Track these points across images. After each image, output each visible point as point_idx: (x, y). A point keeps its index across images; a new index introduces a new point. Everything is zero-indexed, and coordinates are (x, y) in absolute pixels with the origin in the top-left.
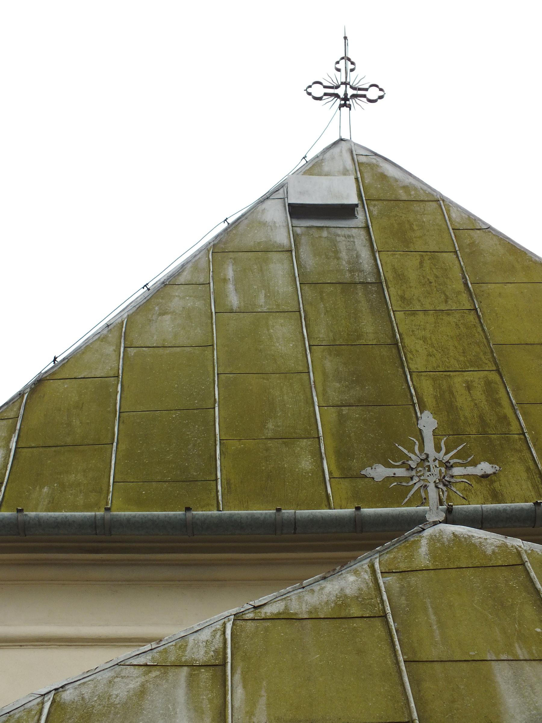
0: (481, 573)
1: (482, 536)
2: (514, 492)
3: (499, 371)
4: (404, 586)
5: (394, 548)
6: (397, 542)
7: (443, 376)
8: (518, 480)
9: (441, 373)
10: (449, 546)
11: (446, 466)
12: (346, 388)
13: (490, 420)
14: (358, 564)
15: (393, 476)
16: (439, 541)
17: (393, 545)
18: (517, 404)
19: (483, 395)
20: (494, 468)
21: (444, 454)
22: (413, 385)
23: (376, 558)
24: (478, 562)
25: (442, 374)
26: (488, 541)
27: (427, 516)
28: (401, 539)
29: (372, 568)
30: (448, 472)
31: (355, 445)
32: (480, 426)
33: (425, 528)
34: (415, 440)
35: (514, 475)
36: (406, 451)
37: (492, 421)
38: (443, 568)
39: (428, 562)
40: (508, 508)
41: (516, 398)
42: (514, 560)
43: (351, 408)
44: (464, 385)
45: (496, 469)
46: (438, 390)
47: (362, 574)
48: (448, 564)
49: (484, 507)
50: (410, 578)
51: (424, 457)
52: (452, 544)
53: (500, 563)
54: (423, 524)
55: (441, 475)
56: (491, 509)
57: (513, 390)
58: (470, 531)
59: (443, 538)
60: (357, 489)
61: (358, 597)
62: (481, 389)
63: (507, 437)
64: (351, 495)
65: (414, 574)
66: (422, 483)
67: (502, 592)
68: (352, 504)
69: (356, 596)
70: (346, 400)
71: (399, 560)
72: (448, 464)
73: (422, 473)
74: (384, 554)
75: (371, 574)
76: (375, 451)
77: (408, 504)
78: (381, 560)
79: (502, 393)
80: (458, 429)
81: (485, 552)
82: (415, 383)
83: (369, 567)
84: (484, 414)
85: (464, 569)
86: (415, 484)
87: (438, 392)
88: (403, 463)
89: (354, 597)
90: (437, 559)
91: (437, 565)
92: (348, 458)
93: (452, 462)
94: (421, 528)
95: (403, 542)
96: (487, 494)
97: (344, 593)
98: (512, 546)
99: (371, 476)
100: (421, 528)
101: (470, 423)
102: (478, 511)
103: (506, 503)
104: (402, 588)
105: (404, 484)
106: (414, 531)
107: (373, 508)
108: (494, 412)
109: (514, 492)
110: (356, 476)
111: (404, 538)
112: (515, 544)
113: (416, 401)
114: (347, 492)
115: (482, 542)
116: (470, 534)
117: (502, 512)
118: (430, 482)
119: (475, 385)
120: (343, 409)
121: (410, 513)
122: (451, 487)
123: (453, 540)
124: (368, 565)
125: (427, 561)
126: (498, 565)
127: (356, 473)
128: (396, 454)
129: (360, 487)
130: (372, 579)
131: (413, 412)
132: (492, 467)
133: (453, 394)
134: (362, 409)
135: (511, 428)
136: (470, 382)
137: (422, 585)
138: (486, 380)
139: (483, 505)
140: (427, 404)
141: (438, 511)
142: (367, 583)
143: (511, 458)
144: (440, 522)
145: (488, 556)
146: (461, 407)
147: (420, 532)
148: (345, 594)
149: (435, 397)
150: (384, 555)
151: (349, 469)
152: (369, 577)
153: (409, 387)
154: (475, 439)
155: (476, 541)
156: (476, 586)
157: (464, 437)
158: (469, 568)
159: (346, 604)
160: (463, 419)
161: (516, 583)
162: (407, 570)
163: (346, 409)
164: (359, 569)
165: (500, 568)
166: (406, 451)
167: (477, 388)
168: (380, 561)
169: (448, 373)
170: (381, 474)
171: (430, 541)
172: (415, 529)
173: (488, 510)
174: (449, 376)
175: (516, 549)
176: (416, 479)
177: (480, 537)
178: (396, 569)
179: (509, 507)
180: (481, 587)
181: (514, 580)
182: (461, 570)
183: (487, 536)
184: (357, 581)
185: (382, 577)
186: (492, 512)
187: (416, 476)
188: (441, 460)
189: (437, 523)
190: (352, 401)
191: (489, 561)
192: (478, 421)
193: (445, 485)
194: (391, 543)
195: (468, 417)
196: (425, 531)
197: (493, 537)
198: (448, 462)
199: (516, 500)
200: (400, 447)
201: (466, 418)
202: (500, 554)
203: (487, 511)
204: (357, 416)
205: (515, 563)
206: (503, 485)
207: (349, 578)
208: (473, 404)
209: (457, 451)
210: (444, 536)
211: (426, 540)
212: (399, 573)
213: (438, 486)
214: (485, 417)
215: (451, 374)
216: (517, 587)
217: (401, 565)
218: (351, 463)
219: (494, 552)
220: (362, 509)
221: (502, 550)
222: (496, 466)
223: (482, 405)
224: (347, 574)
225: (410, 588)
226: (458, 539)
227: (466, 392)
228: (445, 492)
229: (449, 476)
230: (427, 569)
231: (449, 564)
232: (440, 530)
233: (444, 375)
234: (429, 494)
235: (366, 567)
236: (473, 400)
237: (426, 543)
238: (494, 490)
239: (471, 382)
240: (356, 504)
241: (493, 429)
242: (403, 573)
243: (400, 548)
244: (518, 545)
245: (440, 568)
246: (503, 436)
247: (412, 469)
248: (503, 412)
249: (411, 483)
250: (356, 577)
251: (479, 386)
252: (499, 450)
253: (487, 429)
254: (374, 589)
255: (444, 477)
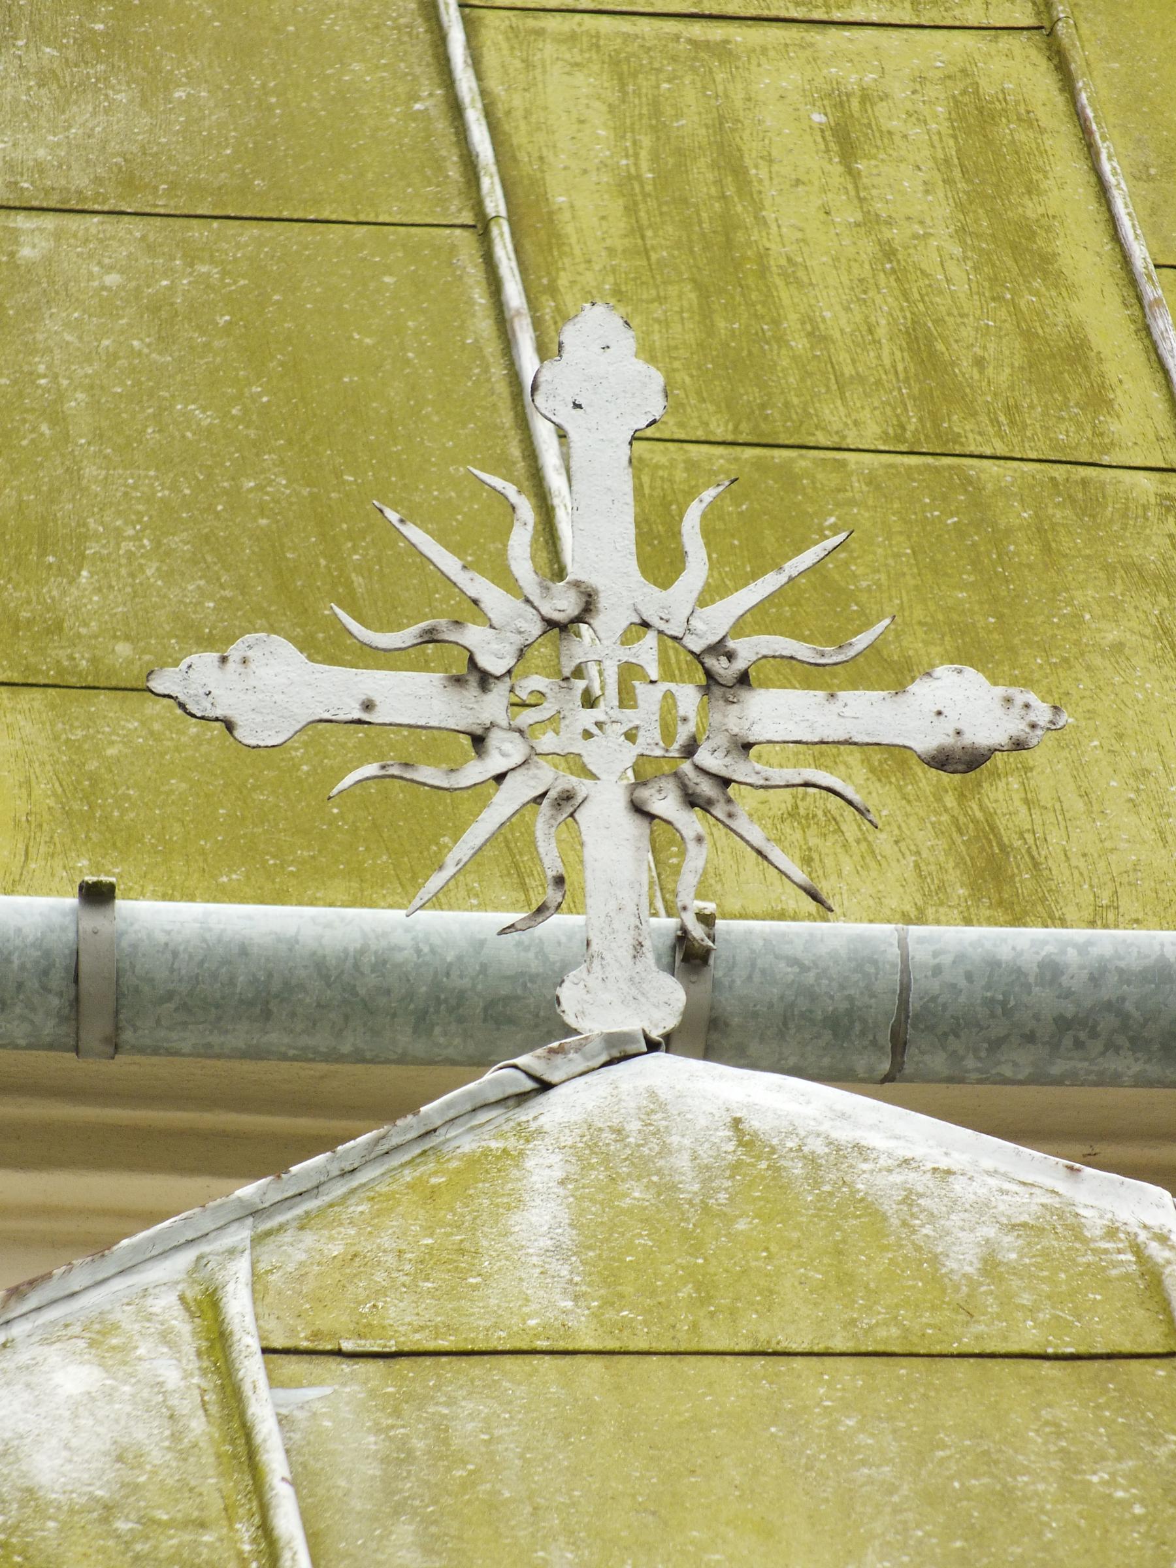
0: (908, 1401)
1: (917, 1152)
2: (1114, 850)
3: (1052, 33)
4: (410, 1452)
5: (353, 1191)
6: (379, 1154)
7: (683, 46)
8: (1146, 772)
9: (671, 26)
10: (706, 1209)
11: (709, 674)
12: (40, 85)
13: (980, 363)
14: (118, 1285)
15: (359, 722)
16: (641, 1166)
17: (343, 1174)
18: (1157, 266)
19: (941, 195)
20: (1017, 710)
21: (695, 594)
22: (483, 93)
23: (232, 1252)
24: (886, 1324)
25: (677, 38)
26: (958, 1185)
27: (564, 993)
28: (395, 1141)
29: (210, 1315)
30: (716, 718)
31: (90, 471)
32: (910, 396)
33: (552, 1078)
34: (511, 491)
35: (1120, 737)
36: (449, 563)
37: (990, 371)
38: (662, 1347)
39: (569, 1304)
40: (1072, 953)
41: (1153, 230)
42: (1123, 1321)
43: (73, 223)
44: (818, 118)
45: (1032, 717)
46: (646, 141)
47: (141, 1351)
48: (694, 1327)
49: (920, 940)
50: (451, 1402)
51: (564, 604)
52: (723, 1197)
53: (1029, 1338)
54: (540, 1051)
55: (668, 734)
56: (960, 958)
57: (1140, 175)
58: (843, 1116)
59: (665, 1150)
60: (92, 765)
61: (108, 1510)
62: (926, 153)
63: (1084, 482)
64: (51, 802)
65: (477, 1372)
66: (544, 777)
67: (1040, 1534)
68: (58, 863)
69: (97, 1500)
70: (40, 167)
71: (380, 1277)
72: (718, 665)
73: (546, 711)
74: (281, 1228)
75: (199, 1354)
76: (217, 515)
77: (436, 902)
78: (263, 1266)
79: (1061, 187)
80: (763, 406)
81: (935, 1260)
82: (496, 86)
83: (187, 1308)
84: (939, 321)
85: (798, 1363)
86: (500, 778)
87: (643, 154)
88: (430, 637)
89: (85, 1510)
90: (628, 1290)
91: (624, 1325)
92: (43, 553)
93: (747, 650)
94: (530, 1076)
95: (407, 1157)
96: (942, 859)
97: (24, 1475)
98: (1112, 1232)
99: (219, 712)
100: (530, 1076)
101: (848, 371)
102: (874, 962)
103: (1063, 923)
104: (399, 1462)
105: (428, 774)
106: (480, 1091)
107: (191, 898)
108: (1003, 313)
109: (1114, 850)
110: (90, 680)
111: (413, 1134)
112: (1132, 1221)
113: (495, 203)
114: (28, 781)
115: (921, 1190)
116: (844, 1134)
117: (1031, 980)
118: (594, 777)
119: (886, 125)
120: (16, 229)
121: (433, 951)
122: (730, 815)
123: (736, 1167)
124: (182, 1298)
125: (565, 1292)
126: (1015, 1348)
127: (94, 660)
128: (354, 549)
129: (111, 751)
130: (203, 1392)
131: (474, 273)
132: (1008, 700)
133: (739, 172)
134: (144, 238)
135: (1114, 426)
136: (855, 103)
137: (527, 1449)
138: (964, 92)
139: (915, 930)
140: (570, 229)
141: (640, 967)
142: (171, 1417)
143: (1103, 625)
144: (652, 1046)
145: (957, 1289)
146: (789, 260)
147: (522, 1098)
148: (27, 1483)
149: (626, 184)
150: (287, 1237)
151: (48, 631)
152: (187, 1375)
153: (456, 109)
154: (872, 480)
155: (883, 1180)
156: (870, 1481)
157: (804, 461)
158: (828, 1361)
159: (31, 1551)
160: (800, 344)
161: (1133, 1479)
162: (431, 1346)
163: (41, 230)
164: (124, 1317)
165: (1025, 1366)
166: (449, 563)
167: (897, 138)
168: (257, 1279)
169: (717, 32)
170: (278, 697)
171: (587, 1167)
172: (490, 1082)
173: (946, 960)
174: (722, 51)
175: (1138, 1250)
176: (507, 747)
177: (906, 1162)
178: (360, 1336)
179: (1082, 949)
180: (905, 1489)
181: (1119, 1459)
182: (782, 1364)
183: (955, 1155)
184: (109, 1395)
185: (270, 1377)
186: (969, 977)
187: (511, 729)
188: (675, 629)
189: (632, 1049)
190: (81, 180)
191: (962, 1317)
192: (900, 367)
193: (691, 800)
194: (331, 1161)
195: (837, 335)
196: (552, 1094)
197: (988, 1164)
198: (718, 648)
199: (1124, 903)
200: (413, 533)
201: (817, 337)
202: (1032, 1276)
203: (937, 970)
204: (112, 279)
205: (1127, 1347)
206: (1045, 797)
207: (59, 1377)
208: (868, 248)
209: (783, 578)
210: (674, 1140)
211: (555, 1159)
212: (381, 1363)
213: (645, 802)
214: (945, 340)
215: (738, 34)
216: (1138, 1510)
217: (392, 1313)
218: (64, 593)
219: (991, 1265)
220: (119, 903)
221: (1045, 1254)
222: (1032, 697)
223: (928, 259)
224: (46, 1350)
225: (449, 1469)
226: (763, 1165)
227: (828, 167)
228: (692, 846)
229: (721, 740)
230: (561, 1345)
231: (705, 1324)
232: (652, 1095)
233: (690, 41)
234: (589, 853)
235: (166, 1304)
236: (870, 222)
237: (559, 1174)
238: (988, 831)
239: (866, 98)
240: (83, 863)
241: (995, 421)
242: (404, 1362)
243: (389, 1197)
244: (1149, 1222)
245: (643, 1346)
246: (1059, 471)
247: (485, 680)
248: (1061, 318)
249: (476, 771)
250: (106, 1369)
251: (915, 131)
252: (1030, 567)
253: (957, 423)
254: (218, 1456)
255: (690, 749)
